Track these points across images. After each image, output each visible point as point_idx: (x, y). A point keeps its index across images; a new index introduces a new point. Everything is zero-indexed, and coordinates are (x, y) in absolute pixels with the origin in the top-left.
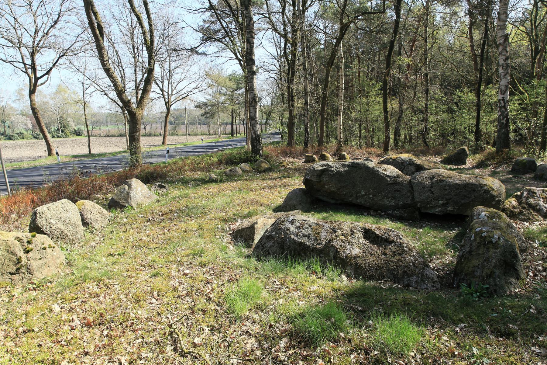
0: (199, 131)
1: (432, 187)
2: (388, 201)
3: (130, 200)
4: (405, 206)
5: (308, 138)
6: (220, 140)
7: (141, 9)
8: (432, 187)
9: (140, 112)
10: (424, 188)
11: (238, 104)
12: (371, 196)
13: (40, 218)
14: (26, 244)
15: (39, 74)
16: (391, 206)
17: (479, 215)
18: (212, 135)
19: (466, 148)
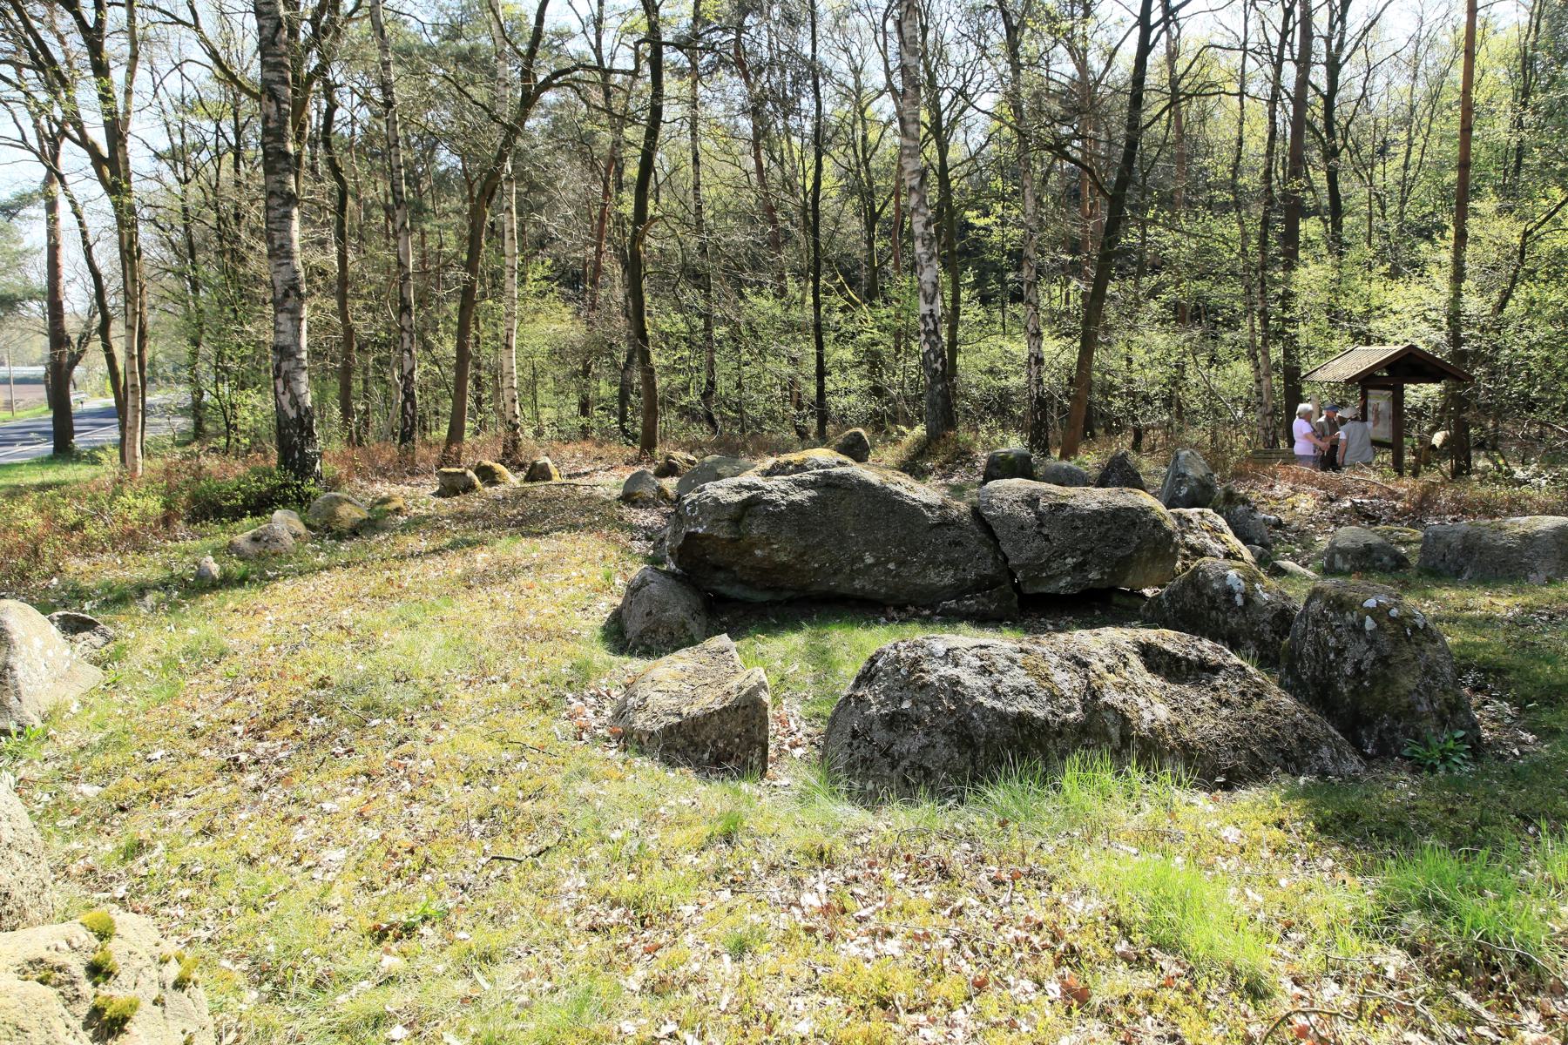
1: (1041, 525)
2: (938, 575)
3: (12, 702)
4: (980, 585)
5: (413, 418)
8: (1041, 525)
10: (1022, 528)
12: (891, 566)
14: (86, 987)
15: (244, 97)
16: (945, 587)
17: (1224, 577)
19: (860, 430)
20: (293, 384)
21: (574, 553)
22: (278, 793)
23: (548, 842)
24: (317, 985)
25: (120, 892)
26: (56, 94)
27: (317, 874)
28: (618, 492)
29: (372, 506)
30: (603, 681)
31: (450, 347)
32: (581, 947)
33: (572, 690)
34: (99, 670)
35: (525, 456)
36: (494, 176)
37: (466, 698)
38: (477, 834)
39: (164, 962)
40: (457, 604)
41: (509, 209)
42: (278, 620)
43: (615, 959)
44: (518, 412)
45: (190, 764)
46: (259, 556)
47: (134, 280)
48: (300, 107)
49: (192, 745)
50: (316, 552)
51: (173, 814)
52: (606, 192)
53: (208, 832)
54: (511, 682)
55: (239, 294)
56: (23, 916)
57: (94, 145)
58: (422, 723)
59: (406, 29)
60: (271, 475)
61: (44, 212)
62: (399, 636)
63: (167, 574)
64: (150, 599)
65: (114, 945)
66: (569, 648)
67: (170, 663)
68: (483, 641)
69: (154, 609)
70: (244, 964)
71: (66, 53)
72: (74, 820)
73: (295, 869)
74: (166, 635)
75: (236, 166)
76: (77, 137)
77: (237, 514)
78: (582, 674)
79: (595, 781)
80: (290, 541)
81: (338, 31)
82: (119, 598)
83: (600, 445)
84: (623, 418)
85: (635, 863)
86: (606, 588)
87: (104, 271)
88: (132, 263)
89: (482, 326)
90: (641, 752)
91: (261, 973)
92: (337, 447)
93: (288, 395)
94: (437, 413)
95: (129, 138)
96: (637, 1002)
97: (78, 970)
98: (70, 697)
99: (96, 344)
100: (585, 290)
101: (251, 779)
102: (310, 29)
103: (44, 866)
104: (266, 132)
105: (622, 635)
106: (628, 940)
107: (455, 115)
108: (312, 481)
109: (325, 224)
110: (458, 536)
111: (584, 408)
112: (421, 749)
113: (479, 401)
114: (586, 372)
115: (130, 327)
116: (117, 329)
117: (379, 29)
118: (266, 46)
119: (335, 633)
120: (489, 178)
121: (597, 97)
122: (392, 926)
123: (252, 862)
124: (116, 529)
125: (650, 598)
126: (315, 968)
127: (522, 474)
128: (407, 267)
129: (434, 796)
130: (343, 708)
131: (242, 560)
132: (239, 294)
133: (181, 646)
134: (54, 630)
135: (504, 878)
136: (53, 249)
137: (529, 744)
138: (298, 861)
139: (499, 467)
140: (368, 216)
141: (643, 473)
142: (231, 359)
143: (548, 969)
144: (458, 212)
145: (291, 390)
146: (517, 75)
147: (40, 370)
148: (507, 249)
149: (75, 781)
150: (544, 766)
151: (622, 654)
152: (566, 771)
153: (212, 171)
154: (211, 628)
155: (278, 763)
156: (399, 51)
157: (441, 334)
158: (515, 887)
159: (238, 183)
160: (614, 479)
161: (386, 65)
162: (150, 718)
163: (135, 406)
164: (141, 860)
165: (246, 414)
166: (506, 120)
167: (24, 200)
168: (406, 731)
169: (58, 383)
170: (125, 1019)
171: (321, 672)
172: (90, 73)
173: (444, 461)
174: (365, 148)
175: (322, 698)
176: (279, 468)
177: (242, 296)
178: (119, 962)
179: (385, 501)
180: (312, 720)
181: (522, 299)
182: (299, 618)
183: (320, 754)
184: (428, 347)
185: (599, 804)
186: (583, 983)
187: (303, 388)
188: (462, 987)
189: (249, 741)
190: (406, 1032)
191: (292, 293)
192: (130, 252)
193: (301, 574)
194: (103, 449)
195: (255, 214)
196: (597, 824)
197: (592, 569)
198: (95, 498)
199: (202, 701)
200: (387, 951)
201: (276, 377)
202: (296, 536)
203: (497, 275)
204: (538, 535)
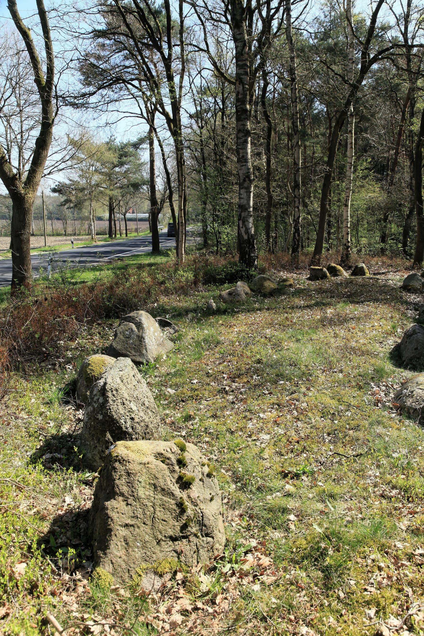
0: (49, 229)
3: (144, 352)
5: (298, 241)
6: (94, 244)
7: (32, 22)
9: (30, 195)
11: (121, 188)
13: (114, 401)
14: (177, 468)
18: (71, 235)
20: (246, 223)
21: (376, 314)
22: (241, 406)
23: (360, 451)
24: (259, 489)
25: (184, 433)
26: (154, 91)
27: (258, 443)
28: (400, 284)
29: (279, 282)
30: (390, 380)
31: (316, 206)
32: (376, 503)
33: (374, 382)
34: (172, 344)
35: (352, 262)
36: (344, 113)
37: (322, 378)
38: (327, 441)
39: (203, 465)
40: (318, 333)
41: (351, 132)
42: (240, 331)
43: (394, 512)
44: (349, 240)
45: (207, 388)
46: (231, 301)
47: (182, 175)
48: (252, 86)
49: (208, 380)
50: (255, 302)
51: (202, 407)
52: (403, 119)
53: (214, 416)
54: (344, 374)
55: (223, 180)
56: (152, 434)
57: (167, 113)
58: (302, 386)
59: (301, 38)
60: (236, 265)
61: (148, 146)
62: (292, 345)
63: (196, 306)
64: (190, 316)
65: (186, 454)
66: (373, 361)
67: (198, 343)
68: (330, 351)
69: (191, 321)
70: (230, 473)
71: (157, 71)
72: (166, 402)
73: (249, 439)
74: (196, 332)
75: (222, 119)
76: (161, 110)
77: (222, 282)
78: (379, 375)
79: (385, 427)
80: (244, 296)
81: (270, 43)
82: (180, 314)
83: (391, 258)
84: (405, 245)
85: (406, 469)
86: (391, 333)
87: (170, 171)
88: (182, 167)
89: (332, 195)
90: (409, 418)
91: (236, 479)
92: (262, 253)
93: (244, 228)
94: (308, 239)
95: (181, 109)
96: (404, 534)
97: (174, 461)
98: (163, 353)
99: (167, 204)
100: (388, 175)
101: (230, 398)
102: (257, 45)
103: (158, 417)
104: (238, 100)
105: (398, 357)
106: (401, 505)
107: (324, 82)
108: (253, 269)
109: (261, 145)
110: (318, 300)
111: (383, 239)
112: (302, 399)
113: (329, 233)
114: (385, 219)
115: (180, 196)
116: (175, 197)
117: (289, 38)
118: (239, 56)
119: (263, 340)
120: (340, 116)
121: (402, 62)
122: (290, 472)
123: (232, 433)
124: (177, 284)
125: (417, 341)
126: (258, 482)
127: (350, 272)
128: (299, 165)
129: (307, 420)
130: (268, 374)
131: (224, 302)
132: (223, 180)
133: (202, 337)
134: (157, 325)
135: (340, 463)
136: (152, 162)
137: (352, 404)
138: (250, 436)
139: (339, 267)
140: (280, 139)
141: (414, 275)
142: (219, 211)
143: (360, 509)
144: (323, 135)
145: (245, 226)
146: (360, 55)
147: (147, 215)
148: (348, 153)
149: (166, 386)
150: (359, 415)
151: (400, 367)
152: (370, 420)
153: (213, 121)
154: (213, 331)
155: (241, 393)
156: (298, 50)
157: (312, 199)
158: (345, 469)
159: (223, 126)
160: (398, 277)
161: (292, 59)
162: (192, 366)
163: (182, 232)
164: (191, 423)
165: (225, 236)
166: (351, 82)
167: (141, 141)
168: (295, 388)
169: (154, 221)
170: (190, 484)
171: (258, 357)
172: (166, 80)
173: (312, 263)
174: (281, 103)
175: (259, 367)
176: (240, 262)
177: (224, 182)
178: (188, 461)
179: (285, 280)
180: (254, 377)
181: (355, 180)
182: (248, 331)
183: (258, 392)
184: (305, 205)
185: (387, 439)
186: (377, 519)
187: (251, 225)
188: (320, 506)
189: (229, 382)
190: (296, 518)
191: (247, 179)
192: (181, 162)
193: (249, 311)
194: (170, 250)
195: (231, 142)
196: (386, 448)
197: (385, 322)
198: (169, 271)
199: (210, 362)
200: (288, 483)
201: (239, 220)
202: (246, 294)
203: (342, 168)
204: (358, 303)
